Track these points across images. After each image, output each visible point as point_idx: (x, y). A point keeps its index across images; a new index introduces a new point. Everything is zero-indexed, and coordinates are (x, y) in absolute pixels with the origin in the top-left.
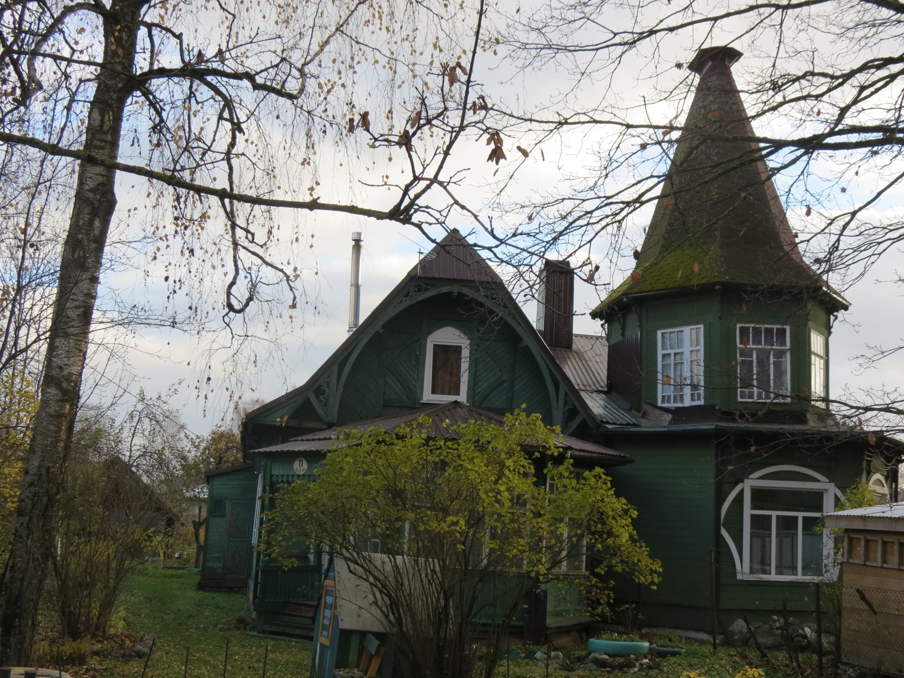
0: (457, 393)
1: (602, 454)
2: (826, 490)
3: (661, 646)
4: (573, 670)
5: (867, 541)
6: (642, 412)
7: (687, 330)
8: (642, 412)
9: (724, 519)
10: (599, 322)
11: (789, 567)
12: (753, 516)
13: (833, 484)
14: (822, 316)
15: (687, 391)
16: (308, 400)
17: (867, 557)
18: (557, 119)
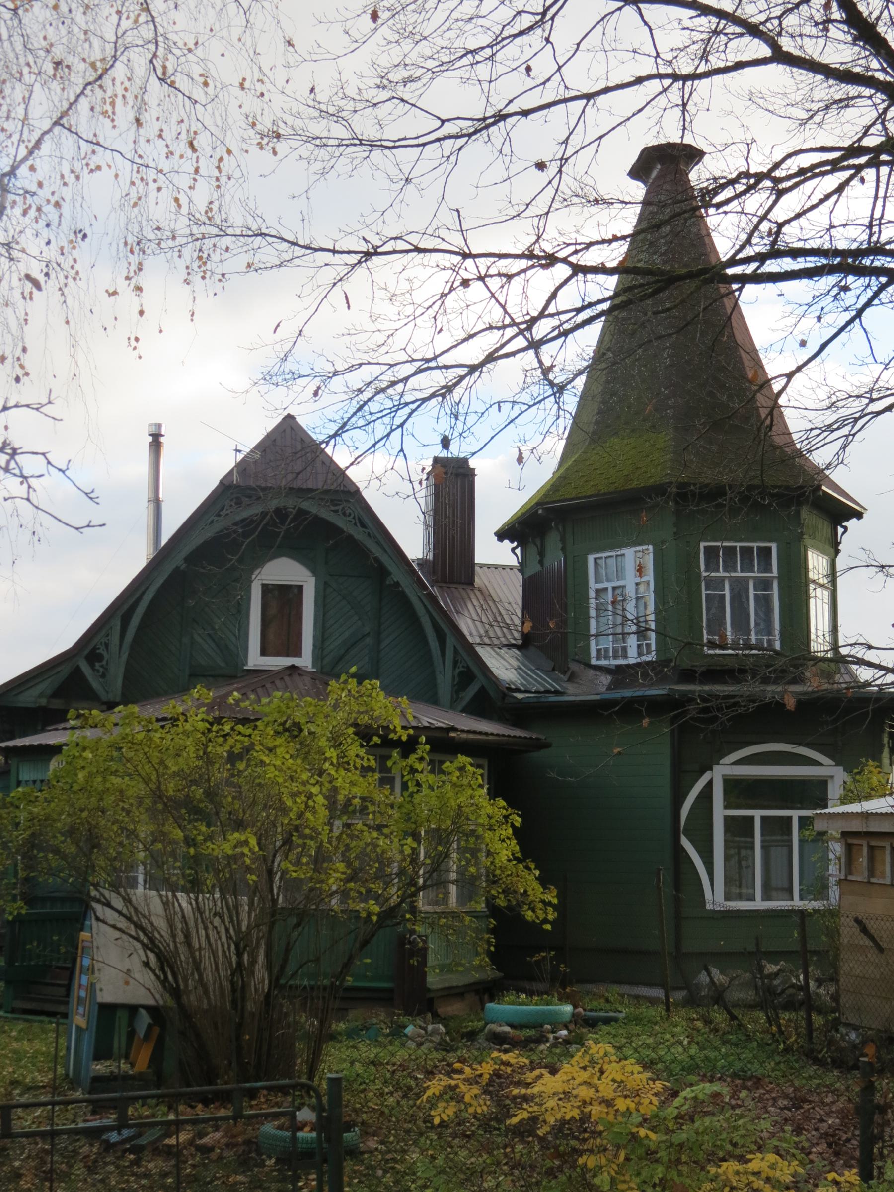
0: (298, 653)
1: (503, 735)
2: (832, 777)
3: (591, 1010)
4: (453, 1049)
5: (871, 849)
6: (569, 674)
7: (629, 553)
8: (569, 674)
9: (686, 824)
10: (507, 545)
11: (783, 889)
12: (726, 818)
13: (841, 768)
14: (825, 527)
15: (632, 642)
16: (78, 670)
17: (872, 872)
18: (364, 247)
